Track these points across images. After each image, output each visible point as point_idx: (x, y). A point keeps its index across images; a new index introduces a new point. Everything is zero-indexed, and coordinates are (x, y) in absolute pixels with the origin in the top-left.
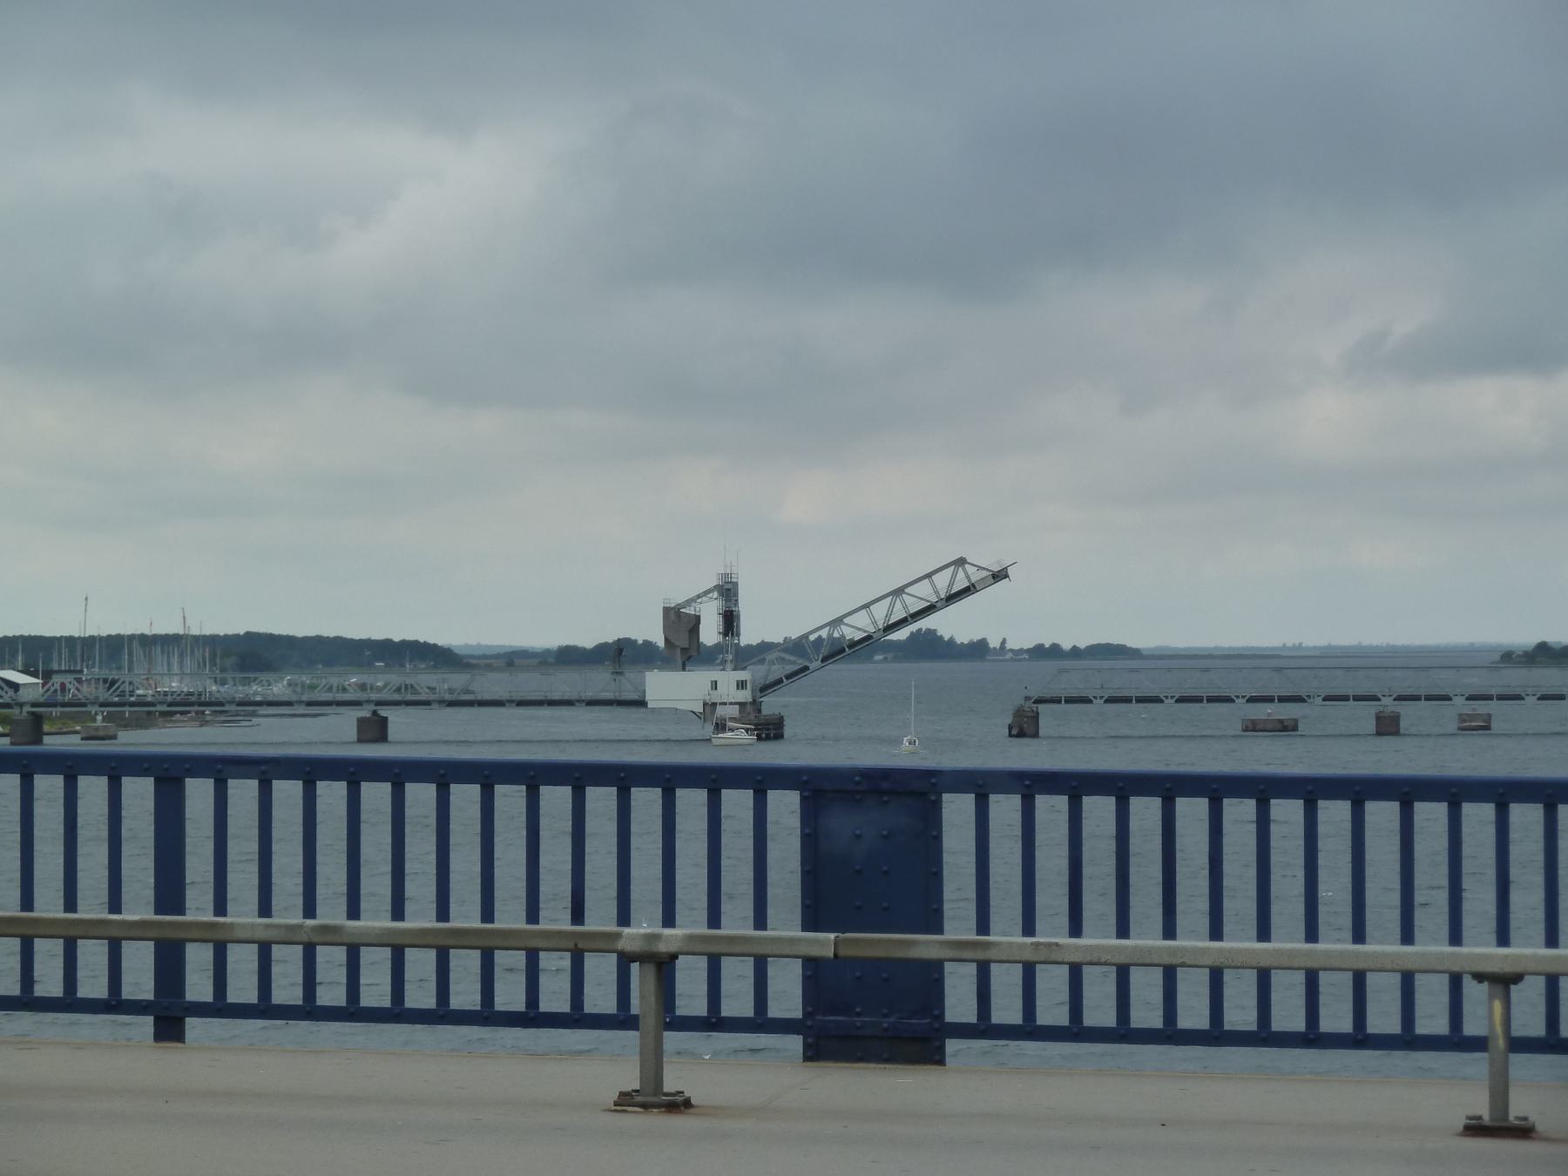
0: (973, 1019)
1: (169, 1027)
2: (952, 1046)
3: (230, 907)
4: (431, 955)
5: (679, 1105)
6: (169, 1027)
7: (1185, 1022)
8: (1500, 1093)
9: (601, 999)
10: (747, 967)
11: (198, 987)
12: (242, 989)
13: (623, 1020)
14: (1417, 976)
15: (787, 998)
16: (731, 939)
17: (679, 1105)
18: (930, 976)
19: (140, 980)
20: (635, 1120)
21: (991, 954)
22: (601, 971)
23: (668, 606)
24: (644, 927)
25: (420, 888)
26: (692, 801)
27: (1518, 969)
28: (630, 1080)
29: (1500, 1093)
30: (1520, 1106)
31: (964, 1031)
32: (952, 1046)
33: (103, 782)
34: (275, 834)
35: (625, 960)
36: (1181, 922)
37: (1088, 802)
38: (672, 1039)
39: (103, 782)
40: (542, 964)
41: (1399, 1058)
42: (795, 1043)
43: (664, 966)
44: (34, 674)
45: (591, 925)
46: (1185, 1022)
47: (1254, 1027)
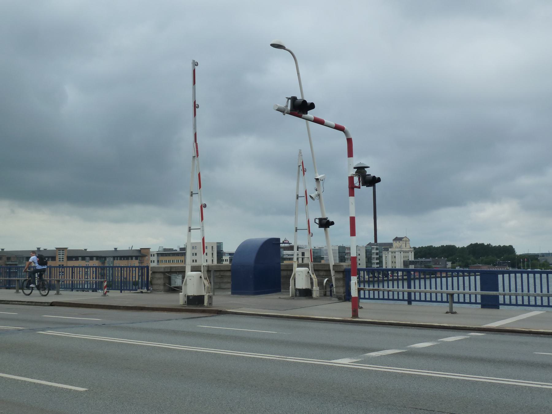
0: (457, 301)
1: (410, 302)
2: (500, 306)
3: (524, 292)
4: (547, 298)
5: (455, 313)
6: (410, 302)
7: (427, 299)
8: (451, 308)
9: (445, 299)
10: (424, 294)
11: (413, 298)
12: (418, 298)
13: (447, 302)
14: (465, 295)
15: (479, 300)
16: (438, 291)
17: (455, 313)
18: (497, 297)
19: (406, 297)
20: (450, 314)
21: (379, 290)
22: (445, 296)
23: (338, 258)
24: (450, 290)
25: (68, 277)
26: (506, 276)
27: (454, 293)
28: (448, 310)
29: (451, 308)
30: (454, 310)
31: (502, 304)
32: (500, 306)
33: (508, 275)
34: (523, 281)
35: (447, 294)
36: (443, 288)
37: (511, 275)
38: (454, 305)
39: (508, 275)
40: (399, 293)
41: (515, 307)
42: (480, 306)
43: (452, 295)
44: (105, 269)
45: (512, 292)
46: (427, 299)
47: (534, 304)
